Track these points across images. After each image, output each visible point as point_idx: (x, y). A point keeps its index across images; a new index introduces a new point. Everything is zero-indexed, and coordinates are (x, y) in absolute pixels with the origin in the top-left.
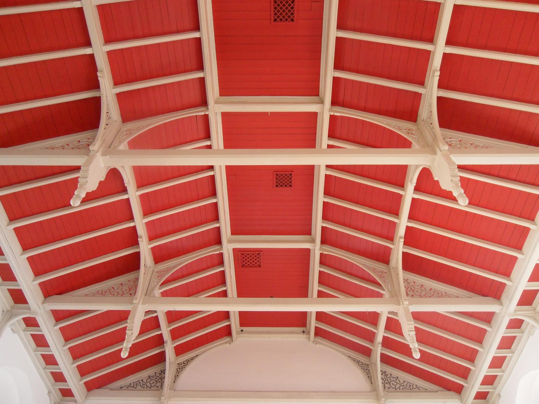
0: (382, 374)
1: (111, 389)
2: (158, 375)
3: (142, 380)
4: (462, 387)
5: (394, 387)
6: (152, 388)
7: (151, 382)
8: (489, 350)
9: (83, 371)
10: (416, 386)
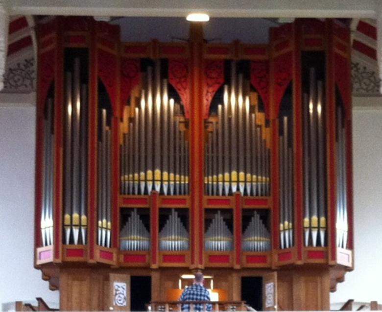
5: (365, 87)
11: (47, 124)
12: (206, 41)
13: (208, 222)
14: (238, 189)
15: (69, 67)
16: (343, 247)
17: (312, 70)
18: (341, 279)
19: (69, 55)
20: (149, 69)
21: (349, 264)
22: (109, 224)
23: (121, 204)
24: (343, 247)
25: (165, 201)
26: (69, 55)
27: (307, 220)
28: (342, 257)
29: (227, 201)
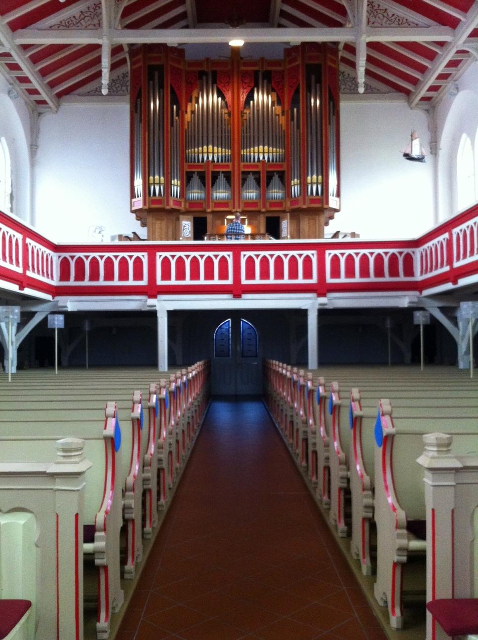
0: (368, 5)
1: (79, 95)
2: (93, 10)
3: (74, 17)
4: (435, 54)
6: (119, 93)
7: (117, 86)
8: (441, 67)
9: (44, 73)
10: (407, 20)
11: (137, 116)
12: (242, 58)
13: (244, 180)
14: (264, 158)
15: (151, 78)
16: (333, 195)
17: (313, 77)
18: (332, 218)
19: (151, 70)
20: (204, 78)
21: (337, 208)
22: (179, 182)
23: (186, 169)
24: (333, 195)
25: (215, 166)
26: (151, 70)
27: (309, 178)
28: (333, 202)
29: (257, 166)
